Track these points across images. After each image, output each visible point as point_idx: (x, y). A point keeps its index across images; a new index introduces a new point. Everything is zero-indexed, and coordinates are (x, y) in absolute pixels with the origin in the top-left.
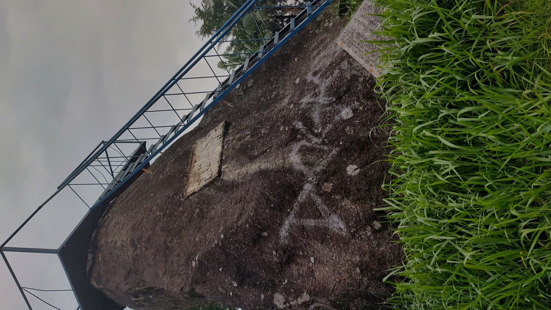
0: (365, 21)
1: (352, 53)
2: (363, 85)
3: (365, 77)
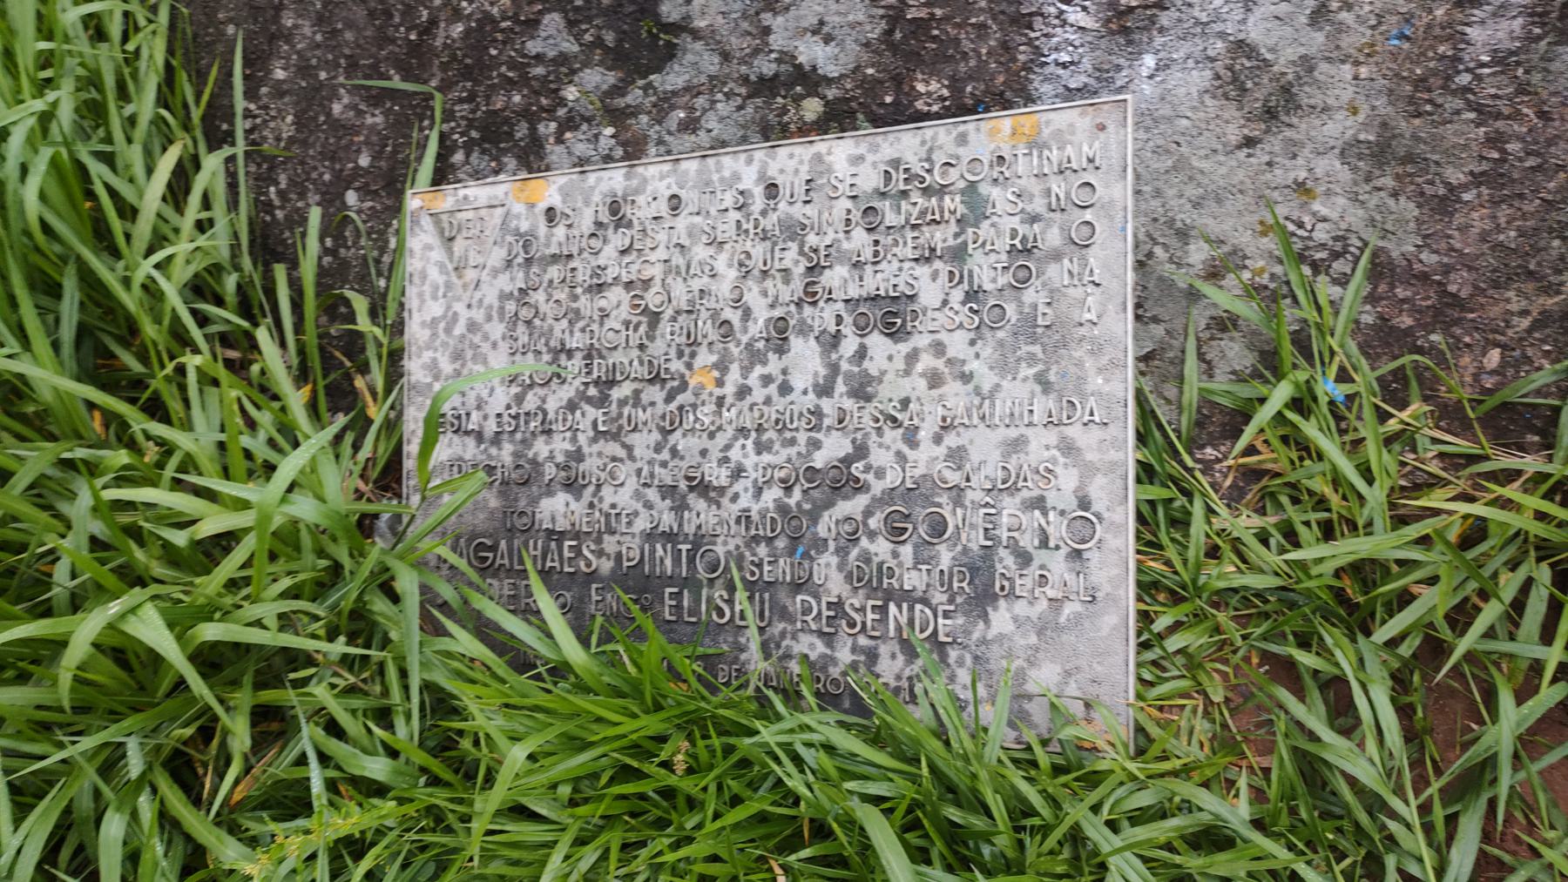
2: (539, 71)
3: (569, 124)
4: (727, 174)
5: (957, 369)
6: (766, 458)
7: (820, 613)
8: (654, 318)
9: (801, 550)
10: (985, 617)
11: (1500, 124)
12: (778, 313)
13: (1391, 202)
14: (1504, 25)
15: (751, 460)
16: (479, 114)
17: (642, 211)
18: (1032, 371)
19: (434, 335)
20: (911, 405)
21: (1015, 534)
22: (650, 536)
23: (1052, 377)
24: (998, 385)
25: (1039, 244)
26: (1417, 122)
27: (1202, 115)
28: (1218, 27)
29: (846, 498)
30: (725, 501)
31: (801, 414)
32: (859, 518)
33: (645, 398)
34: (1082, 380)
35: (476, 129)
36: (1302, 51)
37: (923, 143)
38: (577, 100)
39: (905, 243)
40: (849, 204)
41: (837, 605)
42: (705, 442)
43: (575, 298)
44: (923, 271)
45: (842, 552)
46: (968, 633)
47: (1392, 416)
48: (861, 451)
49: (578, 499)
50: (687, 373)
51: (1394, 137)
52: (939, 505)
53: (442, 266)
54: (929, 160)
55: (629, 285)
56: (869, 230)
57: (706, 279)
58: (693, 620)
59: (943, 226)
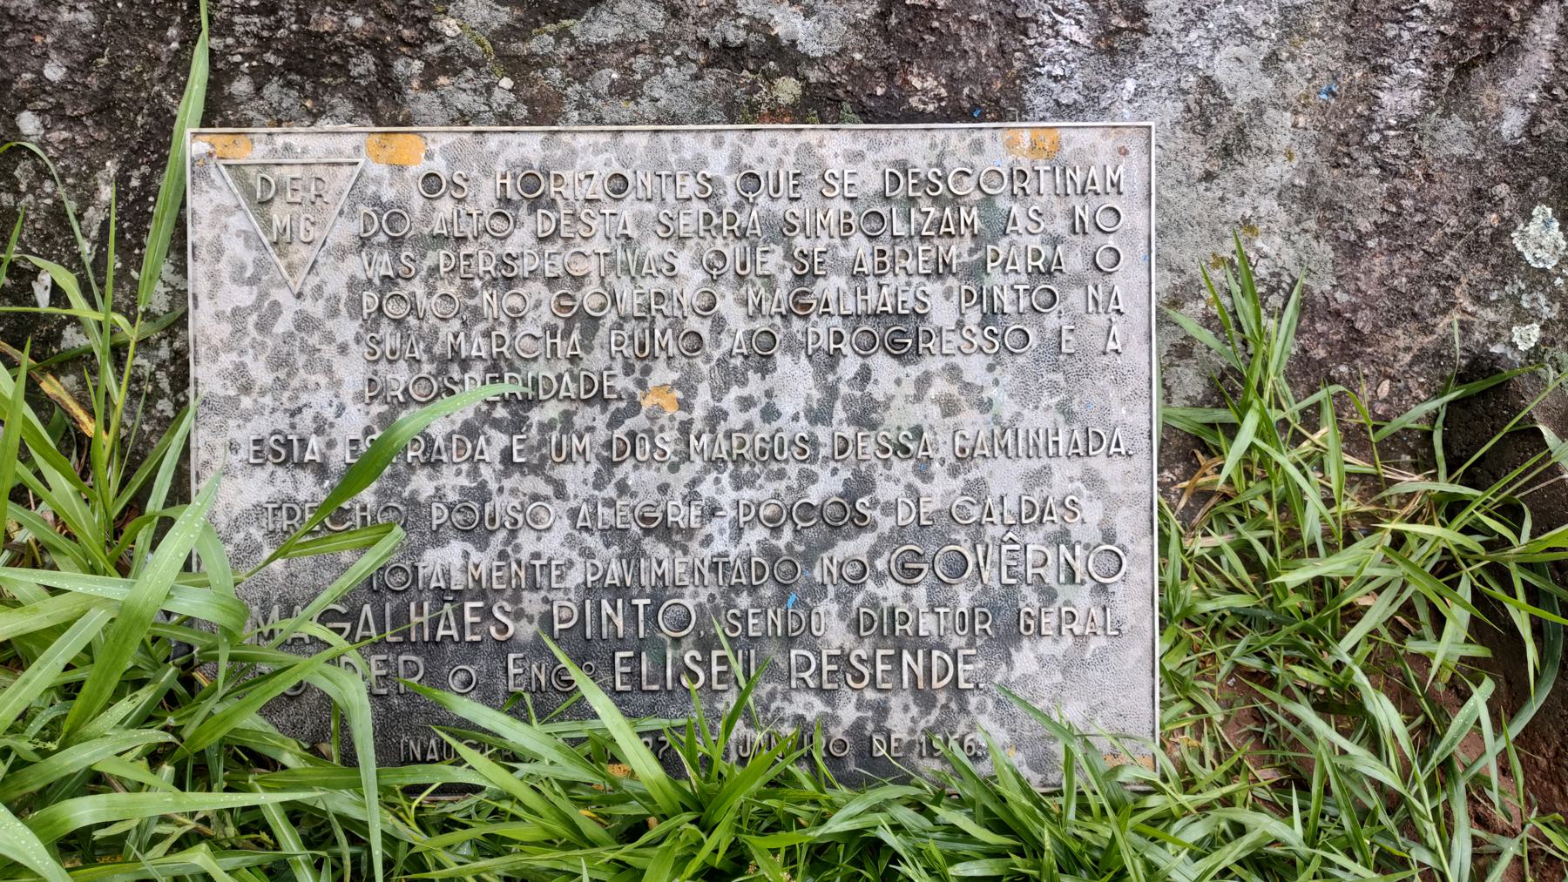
1: (807, 149)
3: (447, 64)
4: (688, 155)
5: (974, 396)
6: (747, 494)
7: (819, 668)
8: (590, 324)
9: (792, 598)
10: (1008, 659)
11: (1397, 181)
12: (760, 325)
13: (1314, 243)
14: (1408, 94)
15: (727, 497)
16: (282, 33)
17: (571, 188)
18: (1056, 400)
19: (239, 332)
20: (925, 435)
21: (1041, 571)
22: (588, 590)
23: (1076, 408)
24: (1019, 414)
25: (1063, 267)
26: (1336, 172)
27: (1172, 145)
28: (1190, 61)
29: (847, 537)
30: (694, 546)
31: (793, 442)
32: (865, 561)
33: (579, 422)
34: (1106, 410)
35: (277, 52)
36: (1255, 94)
37: (933, 146)
38: (458, 37)
39: (916, 255)
40: (846, 207)
41: (842, 659)
42: (665, 476)
43: (472, 293)
44: (934, 288)
45: (843, 598)
46: (989, 677)
47: (1305, 438)
48: (862, 484)
49: (482, 545)
50: (639, 392)
51: (1319, 184)
52: (957, 543)
53: (246, 236)
54: (940, 165)
55: (551, 282)
56: (871, 238)
57: (661, 280)
58: (656, 687)
59: (957, 239)
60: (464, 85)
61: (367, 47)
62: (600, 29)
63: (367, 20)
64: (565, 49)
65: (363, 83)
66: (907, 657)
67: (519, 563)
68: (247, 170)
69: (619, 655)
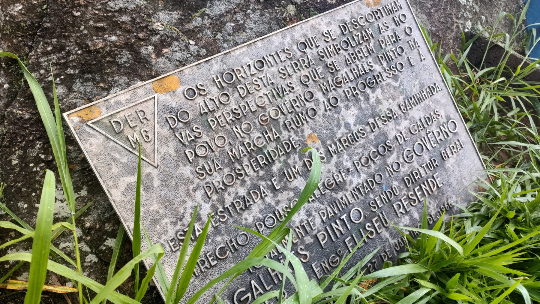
0: (404, 124)
1: (313, 27)
2: (125, 18)
3: (164, 43)
16: (71, 58)
35: (74, 67)
38: (164, 30)
60: (175, 49)
61: (123, 48)
62: (219, 8)
63: (118, 36)
64: (207, 22)
65: (127, 65)
66: (423, 186)
67: (298, 228)
68: (104, 121)
69: (346, 240)
